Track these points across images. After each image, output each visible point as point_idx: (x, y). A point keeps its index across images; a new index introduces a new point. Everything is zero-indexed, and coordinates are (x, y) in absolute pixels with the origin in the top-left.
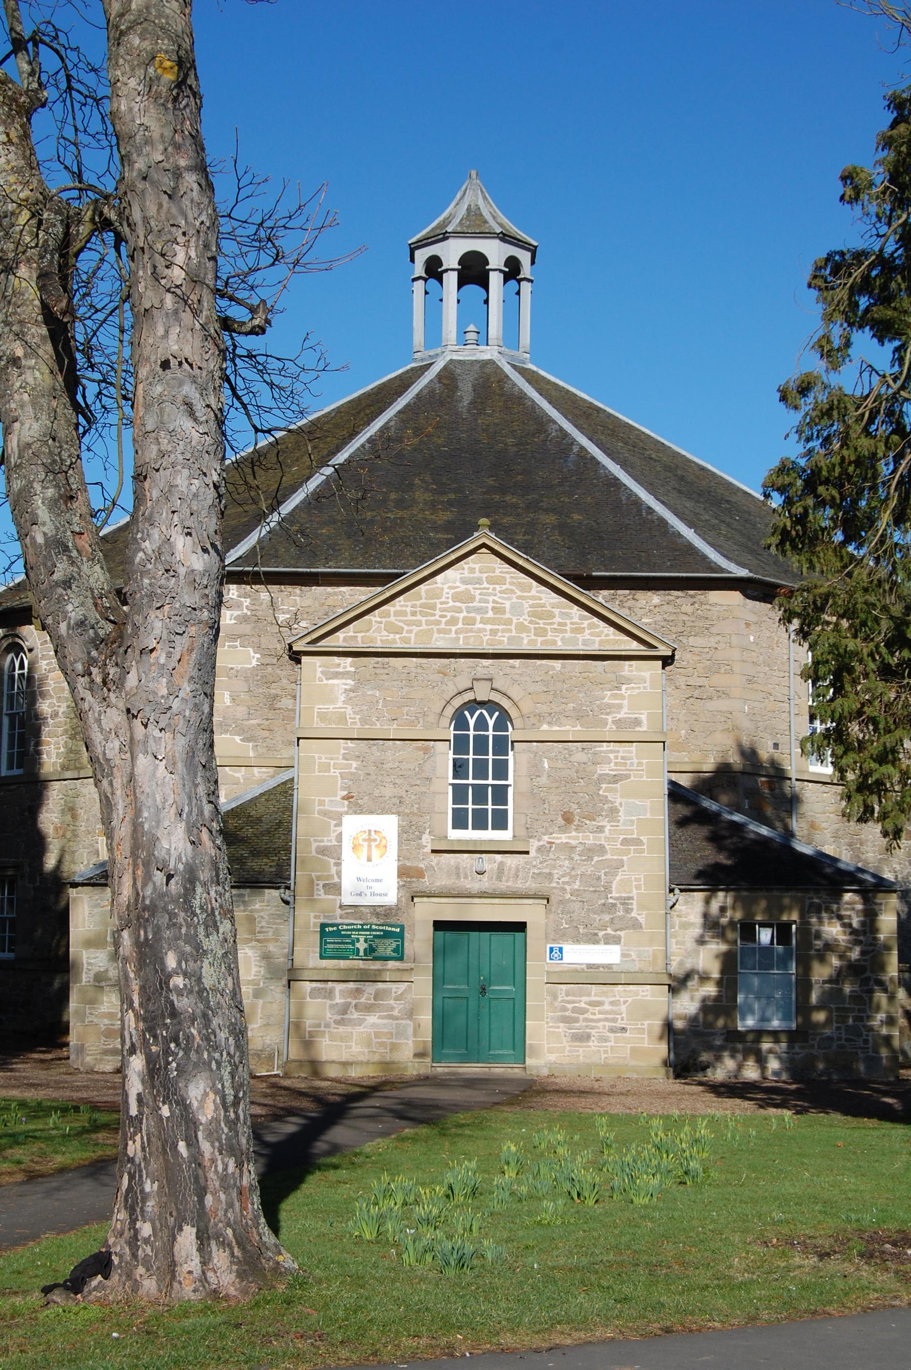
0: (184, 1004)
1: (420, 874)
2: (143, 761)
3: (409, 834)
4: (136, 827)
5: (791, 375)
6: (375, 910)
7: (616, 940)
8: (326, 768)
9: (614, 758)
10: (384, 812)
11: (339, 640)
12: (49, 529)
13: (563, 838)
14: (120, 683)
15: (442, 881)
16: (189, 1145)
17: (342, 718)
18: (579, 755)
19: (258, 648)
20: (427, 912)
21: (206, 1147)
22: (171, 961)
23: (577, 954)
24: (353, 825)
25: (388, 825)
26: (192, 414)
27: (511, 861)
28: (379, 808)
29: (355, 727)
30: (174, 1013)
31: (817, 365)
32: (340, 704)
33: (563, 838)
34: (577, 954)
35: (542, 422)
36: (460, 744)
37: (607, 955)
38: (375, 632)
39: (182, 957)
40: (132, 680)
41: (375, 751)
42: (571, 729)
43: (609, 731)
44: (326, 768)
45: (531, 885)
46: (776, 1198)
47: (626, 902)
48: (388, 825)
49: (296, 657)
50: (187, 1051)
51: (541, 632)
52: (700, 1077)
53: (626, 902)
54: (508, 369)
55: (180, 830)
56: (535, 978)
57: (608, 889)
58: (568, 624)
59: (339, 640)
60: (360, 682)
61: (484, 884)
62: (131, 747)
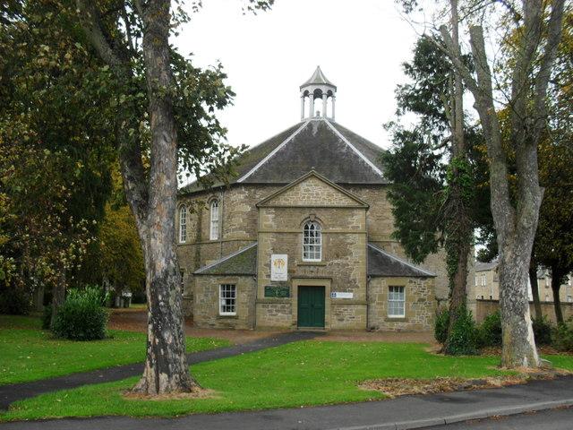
0: (163, 310)
1: (294, 272)
2: (153, 240)
3: (291, 260)
4: (151, 259)
5: (386, 121)
6: (281, 282)
7: (352, 291)
8: (266, 241)
9: (351, 238)
10: (284, 253)
11: (271, 203)
12: (129, 174)
13: (336, 261)
14: (146, 218)
15: (301, 274)
16: (164, 350)
17: (271, 227)
18: (341, 237)
19: (250, 205)
20: (297, 283)
21: (169, 351)
22: (160, 298)
23: (340, 295)
24: (275, 257)
25: (285, 257)
26: (165, 140)
27: (321, 269)
28: (282, 252)
29: (275, 229)
30: (160, 312)
31: (395, 118)
32: (270, 222)
33: (336, 261)
34: (340, 295)
35: (337, 138)
36: (306, 233)
37: (349, 295)
38: (282, 201)
39: (163, 296)
40: (149, 217)
41: (281, 236)
42: (339, 229)
43: (350, 230)
44: (266, 241)
45: (327, 275)
46: (221, 370)
47: (354, 280)
48: (285, 257)
49: (258, 208)
50: (164, 323)
51: (330, 200)
52: (265, 335)
53: (354, 280)
54: (328, 123)
55: (164, 261)
56: (327, 303)
57: (349, 276)
58: (339, 200)
59: (271, 203)
60: (277, 216)
61: (313, 275)
62: (149, 237)
